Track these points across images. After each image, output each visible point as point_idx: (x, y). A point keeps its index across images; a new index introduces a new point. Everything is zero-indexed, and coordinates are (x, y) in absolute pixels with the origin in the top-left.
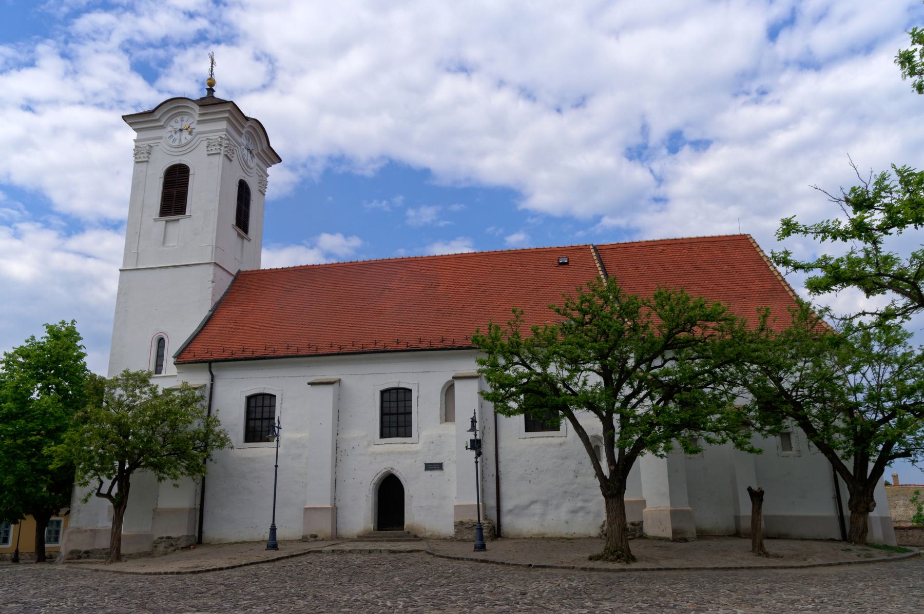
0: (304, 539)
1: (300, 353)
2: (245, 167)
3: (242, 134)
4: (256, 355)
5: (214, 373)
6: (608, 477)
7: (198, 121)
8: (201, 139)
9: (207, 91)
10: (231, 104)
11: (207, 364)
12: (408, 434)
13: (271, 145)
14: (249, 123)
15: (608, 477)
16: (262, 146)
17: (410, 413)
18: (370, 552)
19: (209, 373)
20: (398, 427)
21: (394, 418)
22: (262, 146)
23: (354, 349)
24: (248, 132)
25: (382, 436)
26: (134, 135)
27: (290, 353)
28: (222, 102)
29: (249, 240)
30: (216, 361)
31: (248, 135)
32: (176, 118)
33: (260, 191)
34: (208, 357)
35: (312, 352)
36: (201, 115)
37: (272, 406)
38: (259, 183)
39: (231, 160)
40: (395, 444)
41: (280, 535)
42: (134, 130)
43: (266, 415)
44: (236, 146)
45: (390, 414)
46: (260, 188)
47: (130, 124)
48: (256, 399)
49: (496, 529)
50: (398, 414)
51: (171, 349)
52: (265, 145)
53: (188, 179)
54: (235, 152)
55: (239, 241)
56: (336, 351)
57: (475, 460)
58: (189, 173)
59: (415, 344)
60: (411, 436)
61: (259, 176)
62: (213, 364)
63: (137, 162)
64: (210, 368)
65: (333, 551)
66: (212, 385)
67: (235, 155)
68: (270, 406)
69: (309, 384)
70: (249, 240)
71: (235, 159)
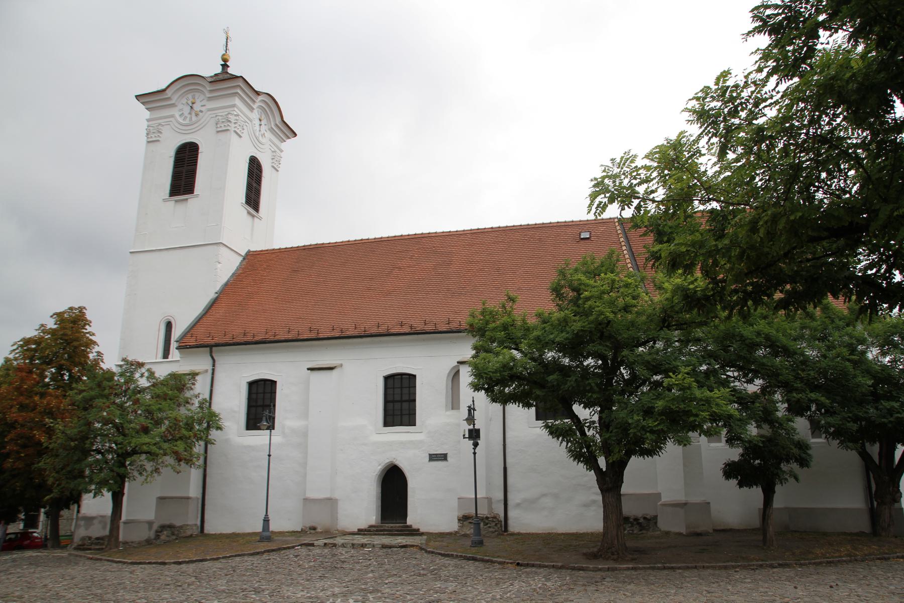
0: (303, 532)
1: (301, 337)
2: (256, 141)
3: (253, 109)
4: (257, 338)
5: (216, 358)
6: (604, 469)
7: (209, 97)
8: (211, 116)
9: (221, 67)
10: (241, 79)
11: (208, 349)
12: (412, 422)
13: (285, 120)
14: (260, 98)
15: (604, 469)
16: (275, 120)
17: (415, 400)
18: (363, 546)
19: (210, 358)
20: (402, 415)
21: (398, 406)
22: (275, 120)
23: (356, 333)
24: (260, 107)
25: (386, 424)
26: (147, 114)
27: (290, 336)
28: (236, 77)
29: (260, 219)
30: (217, 345)
31: (260, 110)
32: (195, 93)
33: (273, 167)
34: (209, 341)
35: (313, 335)
36: (211, 91)
37: (273, 392)
38: (273, 159)
39: (240, 137)
40: (399, 434)
41: (273, 527)
42: (147, 109)
43: (406, 397)
44: (246, 122)
45: (394, 401)
46: (273, 165)
47: (143, 103)
48: (394, 379)
49: (503, 523)
50: (401, 401)
51: (176, 333)
52: (278, 119)
53: (197, 157)
54: (245, 127)
55: (250, 218)
56: (337, 335)
57: (473, 451)
58: (198, 151)
59: (420, 327)
60: (415, 425)
61: (273, 152)
62: (214, 349)
63: (149, 142)
64: (211, 352)
65: (325, 544)
66: (213, 370)
67: (245, 131)
68: (409, 387)
69: (308, 369)
70: (260, 219)
71: (245, 135)
